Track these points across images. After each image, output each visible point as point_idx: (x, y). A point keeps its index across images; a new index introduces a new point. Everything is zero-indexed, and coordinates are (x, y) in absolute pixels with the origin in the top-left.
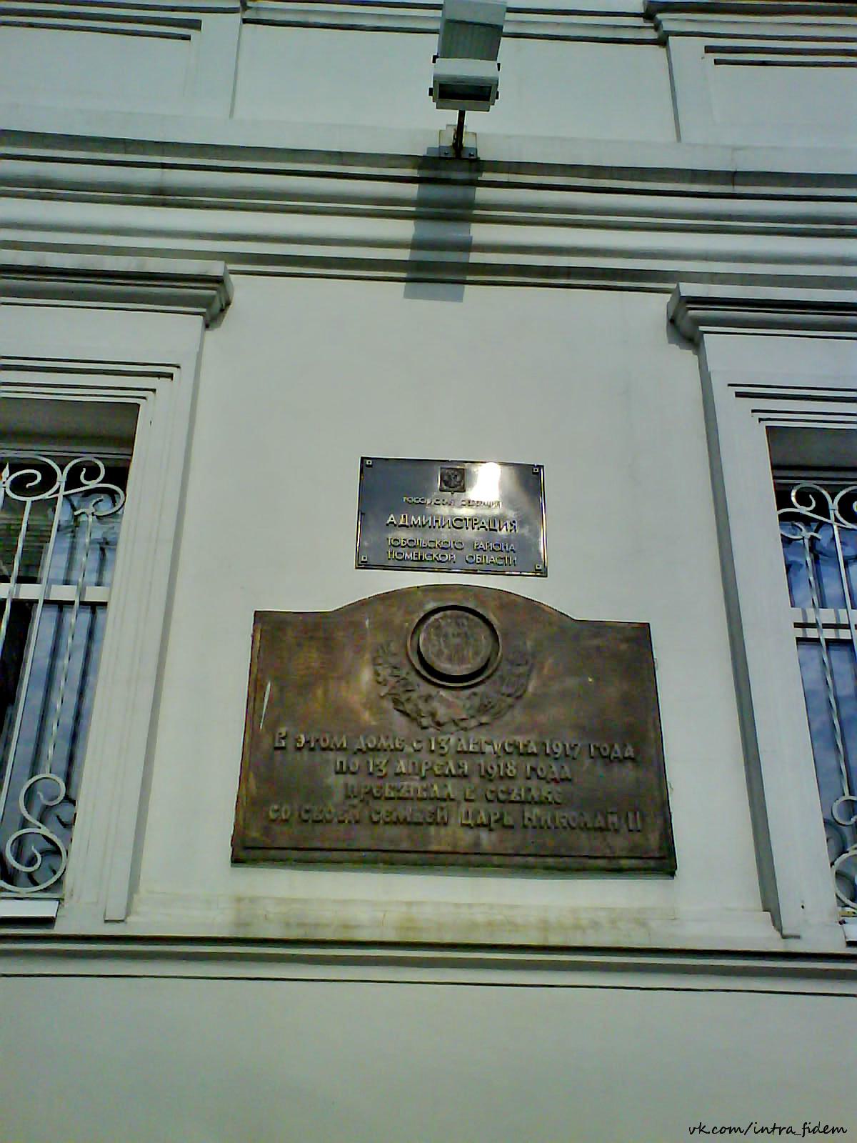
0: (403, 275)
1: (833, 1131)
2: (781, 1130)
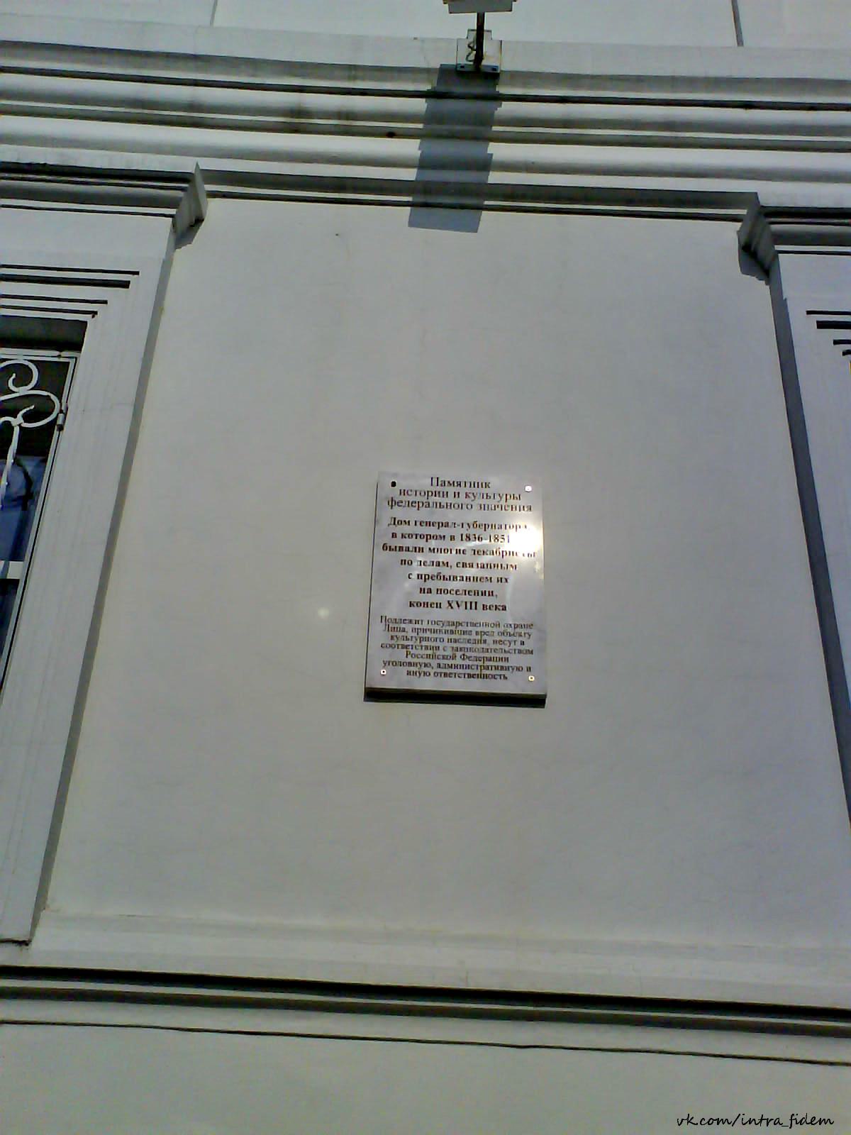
0: (409, 199)
1: (820, 1122)
2: (768, 1122)
